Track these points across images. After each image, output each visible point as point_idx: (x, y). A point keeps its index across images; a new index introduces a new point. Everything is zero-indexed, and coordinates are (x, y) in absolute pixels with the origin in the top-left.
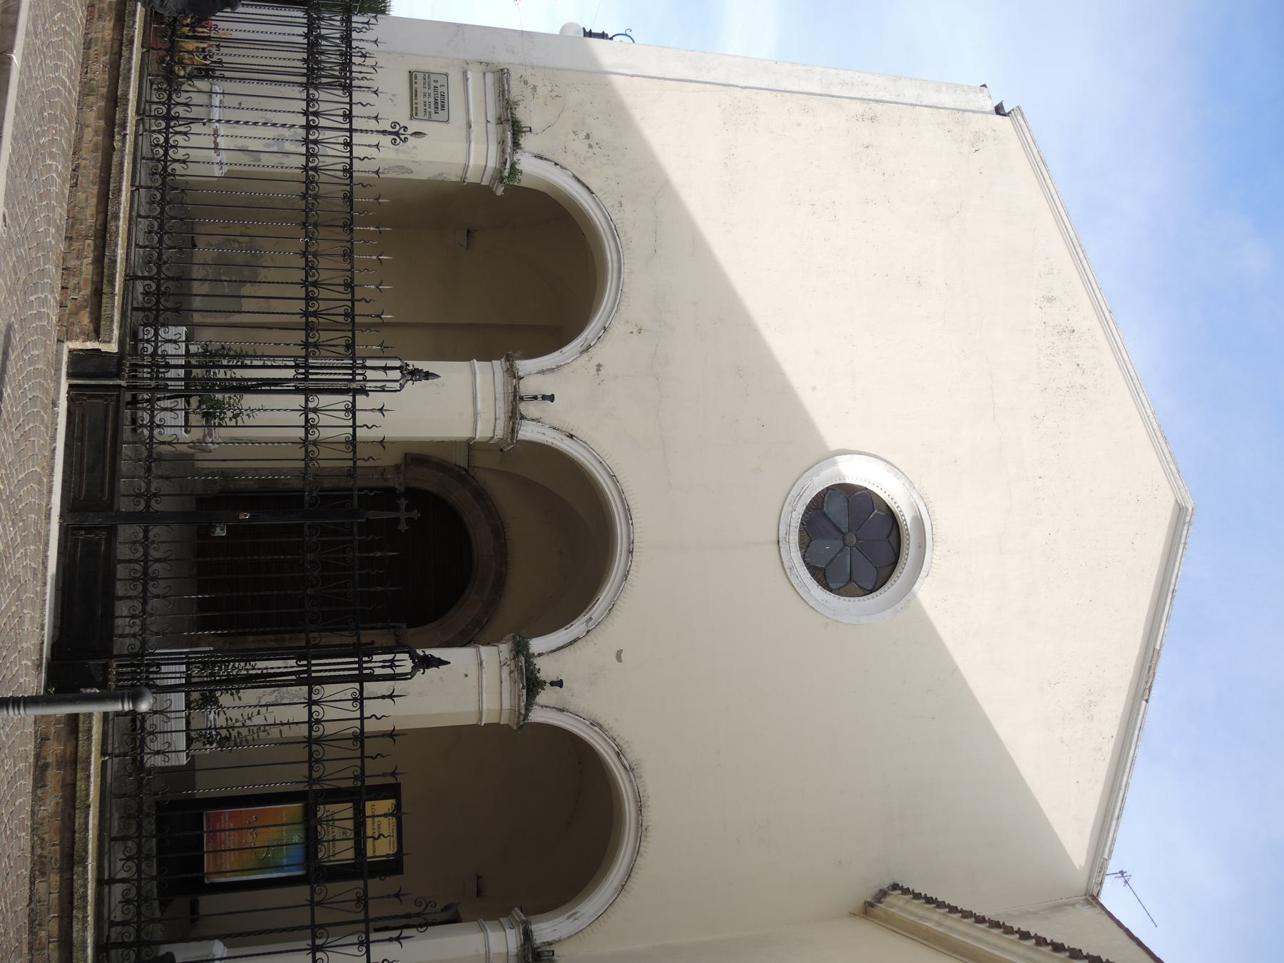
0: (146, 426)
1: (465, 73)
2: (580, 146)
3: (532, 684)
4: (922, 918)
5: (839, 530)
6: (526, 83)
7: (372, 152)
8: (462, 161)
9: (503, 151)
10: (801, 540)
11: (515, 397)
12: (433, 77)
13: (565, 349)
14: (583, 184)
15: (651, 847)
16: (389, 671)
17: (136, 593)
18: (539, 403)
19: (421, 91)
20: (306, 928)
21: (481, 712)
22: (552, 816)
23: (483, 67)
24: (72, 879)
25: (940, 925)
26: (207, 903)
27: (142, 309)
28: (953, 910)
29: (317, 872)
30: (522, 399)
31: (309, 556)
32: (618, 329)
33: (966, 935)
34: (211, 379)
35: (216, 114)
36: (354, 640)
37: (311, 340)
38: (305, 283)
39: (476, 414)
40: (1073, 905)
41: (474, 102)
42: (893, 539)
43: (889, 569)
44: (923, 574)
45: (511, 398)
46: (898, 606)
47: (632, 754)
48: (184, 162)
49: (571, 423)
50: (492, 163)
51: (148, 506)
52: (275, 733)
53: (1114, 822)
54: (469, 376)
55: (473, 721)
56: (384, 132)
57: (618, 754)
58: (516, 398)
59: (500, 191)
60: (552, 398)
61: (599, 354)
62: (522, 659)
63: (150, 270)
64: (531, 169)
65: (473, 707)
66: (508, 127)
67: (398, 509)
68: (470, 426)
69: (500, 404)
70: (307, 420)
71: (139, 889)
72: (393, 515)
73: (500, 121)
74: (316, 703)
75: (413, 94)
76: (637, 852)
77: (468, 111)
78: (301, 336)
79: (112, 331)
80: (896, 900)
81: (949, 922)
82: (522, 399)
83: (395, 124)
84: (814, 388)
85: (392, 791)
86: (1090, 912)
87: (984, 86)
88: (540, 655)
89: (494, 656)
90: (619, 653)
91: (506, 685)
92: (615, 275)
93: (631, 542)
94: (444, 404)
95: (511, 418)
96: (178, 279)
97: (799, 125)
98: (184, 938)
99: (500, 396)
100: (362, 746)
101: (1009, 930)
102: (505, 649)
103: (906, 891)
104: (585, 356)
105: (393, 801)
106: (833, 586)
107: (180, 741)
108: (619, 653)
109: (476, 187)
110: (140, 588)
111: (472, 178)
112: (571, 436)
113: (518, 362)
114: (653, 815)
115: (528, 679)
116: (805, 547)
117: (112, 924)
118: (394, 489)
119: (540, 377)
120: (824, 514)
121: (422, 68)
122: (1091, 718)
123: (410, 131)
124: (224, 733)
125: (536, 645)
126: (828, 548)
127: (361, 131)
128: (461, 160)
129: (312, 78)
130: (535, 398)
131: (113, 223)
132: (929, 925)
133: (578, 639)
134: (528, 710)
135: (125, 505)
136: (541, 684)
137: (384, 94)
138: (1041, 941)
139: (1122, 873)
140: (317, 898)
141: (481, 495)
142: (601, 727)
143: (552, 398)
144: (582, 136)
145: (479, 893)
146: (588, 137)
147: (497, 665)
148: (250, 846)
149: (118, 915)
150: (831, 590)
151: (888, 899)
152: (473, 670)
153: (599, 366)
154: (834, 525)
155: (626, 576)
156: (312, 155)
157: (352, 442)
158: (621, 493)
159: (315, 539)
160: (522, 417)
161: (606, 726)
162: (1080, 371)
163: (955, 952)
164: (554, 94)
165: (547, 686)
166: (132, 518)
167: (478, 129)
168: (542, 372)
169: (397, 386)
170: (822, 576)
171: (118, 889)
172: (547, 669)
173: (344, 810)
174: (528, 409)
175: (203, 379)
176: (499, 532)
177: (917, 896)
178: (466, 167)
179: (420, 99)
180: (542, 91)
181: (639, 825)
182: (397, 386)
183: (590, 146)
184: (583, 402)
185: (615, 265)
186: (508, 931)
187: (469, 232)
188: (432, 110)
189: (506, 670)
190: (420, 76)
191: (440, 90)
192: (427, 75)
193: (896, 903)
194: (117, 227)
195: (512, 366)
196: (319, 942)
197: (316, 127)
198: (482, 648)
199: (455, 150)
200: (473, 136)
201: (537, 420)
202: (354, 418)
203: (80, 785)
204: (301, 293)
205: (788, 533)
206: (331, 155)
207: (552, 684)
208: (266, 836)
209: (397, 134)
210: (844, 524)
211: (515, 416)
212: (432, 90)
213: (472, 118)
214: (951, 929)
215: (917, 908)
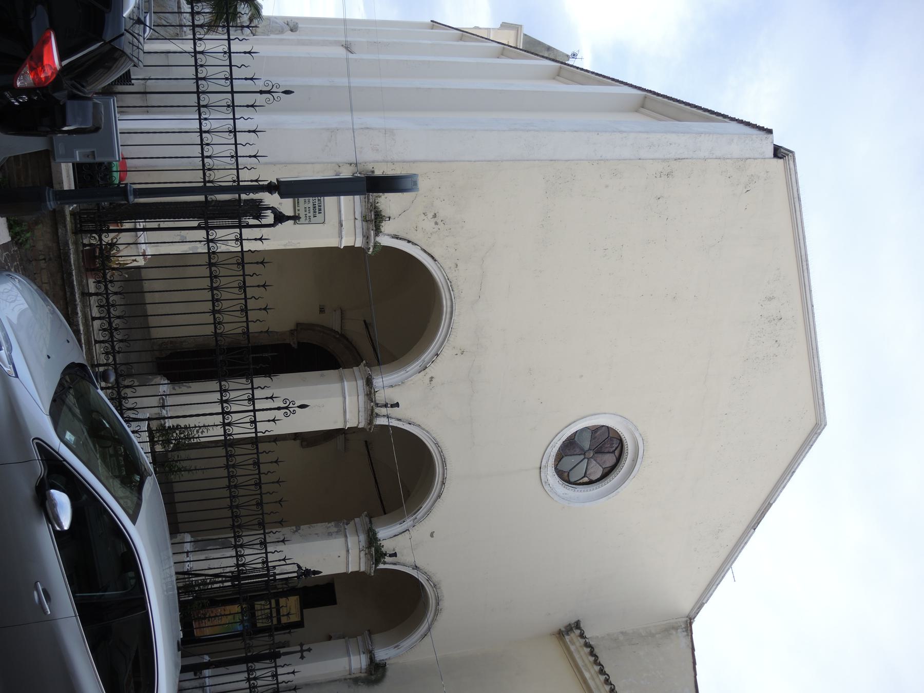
2: (428, 225)
7: (291, 677)
14: (429, 254)
31: (221, 358)
32: (447, 353)
37: (212, 261)
38: (227, 467)
45: (369, 412)
56: (279, 408)
60: (397, 405)
61: (432, 370)
68: (341, 419)
69: (362, 414)
70: (211, 273)
74: (217, 288)
78: (246, 675)
92: (448, 316)
93: (444, 478)
99: (362, 409)
114: (445, 604)
119: (391, 389)
143: (397, 405)
144: (430, 215)
146: (435, 216)
152: (343, 553)
156: (236, 517)
157: (247, 333)
162: (777, 345)
172: (388, 546)
183: (436, 223)
185: (449, 310)
188: (312, 214)
189: (363, 553)
198: (337, 327)
200: (343, 233)
202: (247, 316)
204: (210, 319)
206: (221, 147)
209: (287, 408)
211: (372, 415)
213: (343, 218)
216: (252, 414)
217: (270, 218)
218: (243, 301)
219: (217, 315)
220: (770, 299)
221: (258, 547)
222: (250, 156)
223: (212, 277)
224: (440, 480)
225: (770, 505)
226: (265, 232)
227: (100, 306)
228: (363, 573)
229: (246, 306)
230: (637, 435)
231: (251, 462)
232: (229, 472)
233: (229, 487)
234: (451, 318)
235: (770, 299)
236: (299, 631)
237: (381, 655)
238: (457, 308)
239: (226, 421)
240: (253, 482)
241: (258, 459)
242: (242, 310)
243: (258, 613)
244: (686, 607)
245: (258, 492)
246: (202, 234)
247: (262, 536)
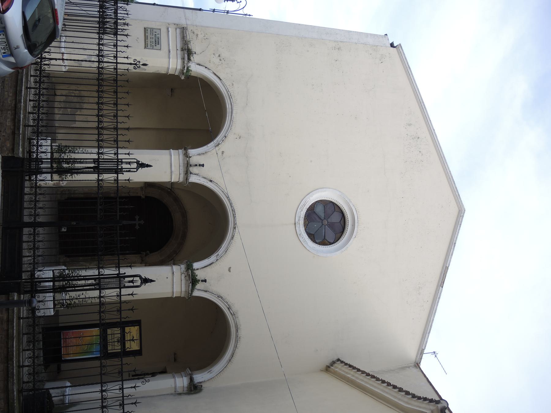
0: (35, 145)
1: (168, 29)
2: (216, 60)
3: (194, 281)
4: (347, 373)
5: (320, 219)
6: (193, 33)
8: (166, 66)
9: (184, 62)
10: (304, 223)
11: (188, 165)
12: (154, 30)
13: (209, 145)
14: (217, 76)
15: (242, 345)
16: (131, 284)
17: (30, 254)
18: (198, 167)
19: (149, 36)
20: (101, 377)
21: (173, 293)
22: (200, 336)
23: (175, 26)
24: (8, 367)
25: (353, 376)
26: (64, 366)
27: (33, 101)
28: (359, 370)
29: (106, 355)
30: (191, 165)
31: (100, 239)
32: (231, 137)
33: (362, 380)
34: (61, 159)
35: (63, 45)
36: (117, 272)
39: (171, 172)
40: (409, 367)
41: (171, 41)
42: (342, 222)
43: (340, 234)
44: (353, 236)
46: (343, 249)
47: (234, 309)
48: (48, 77)
49: (211, 176)
50: (179, 67)
51: (35, 219)
52: (89, 301)
53: (427, 335)
54: (168, 157)
55: (170, 296)
56: (131, 64)
57: (229, 309)
58: (188, 165)
59: (183, 78)
60: (203, 165)
61: (223, 147)
62: (190, 271)
63: (31, 190)
64: (195, 69)
65: (170, 290)
66: (186, 52)
67: (135, 220)
68: (169, 177)
69: (182, 168)
71: (34, 369)
72: (133, 222)
73: (182, 50)
74: (103, 312)
75: (146, 38)
76: (236, 347)
77: (169, 45)
79: (19, 149)
80: (338, 365)
81: (357, 375)
82: (191, 165)
83: (135, 60)
84: (311, 161)
85: (137, 323)
86: (415, 370)
87: (386, 35)
88: (197, 269)
89: (178, 270)
90: (230, 268)
91: (183, 282)
93: (235, 224)
94: (161, 166)
95: (186, 174)
96: (46, 126)
97: (308, 51)
98: (55, 379)
99: (182, 165)
100: (121, 314)
101: (378, 379)
102: (183, 267)
103: (342, 362)
104: (217, 148)
105: (138, 327)
106: (317, 241)
107: (51, 304)
108: (230, 268)
109: (173, 75)
110: (32, 252)
111: (171, 72)
112: (211, 181)
113: (189, 150)
115: (192, 279)
116: (306, 226)
117: (24, 382)
118: (140, 197)
119: (198, 157)
120: (315, 212)
121: (150, 26)
122: (419, 294)
123: (141, 63)
124: (68, 302)
125: (196, 265)
126: (316, 226)
127: (121, 63)
128: (166, 66)
129: (102, 30)
130: (196, 165)
131: (19, 105)
132: (349, 376)
133: (213, 263)
134: (192, 291)
135: (26, 219)
136: (198, 281)
137: (134, 33)
138: (389, 384)
139: (434, 352)
140: (103, 372)
141: (177, 199)
142: (222, 298)
143: (203, 165)
144: (217, 55)
145: (175, 360)
146: (219, 56)
147: (180, 274)
148: (81, 344)
149: (26, 379)
150: (316, 243)
151: (335, 365)
152: (170, 275)
153: (223, 152)
154: (319, 217)
155: (232, 238)
158: (231, 204)
159: (102, 232)
160: (191, 173)
161: (224, 297)
162: (421, 154)
163: (358, 387)
164: (205, 38)
165: (200, 282)
166: (29, 225)
167: (173, 53)
168: (199, 154)
169: (135, 170)
170: (312, 237)
171: (26, 369)
172: (200, 275)
173: (117, 331)
174: (193, 170)
175: (58, 159)
176: (184, 214)
177: (346, 364)
178: (168, 68)
179: (149, 40)
180: (200, 36)
181: (237, 336)
182: (135, 170)
183: (220, 60)
184: (215, 167)
185: (230, 110)
186: (184, 378)
187: (172, 90)
188: (154, 44)
189: (183, 276)
190: (149, 30)
191: (157, 36)
192: (152, 29)
193: (338, 367)
194: (21, 106)
195: (186, 152)
196: (104, 389)
197: (103, 62)
199: (163, 61)
200: (171, 56)
201: (197, 174)
203: (10, 331)
204: (96, 119)
205: (299, 220)
207: (202, 281)
208: (87, 340)
209: (136, 64)
210: (322, 215)
211: (187, 173)
212: (154, 36)
213: (171, 48)
214: (357, 378)
215: (346, 369)
217: (138, 282)
218: (120, 366)
219: (100, 143)
220: (410, 125)
221: (112, 106)
222: (129, 295)
223: (99, 109)
224: (232, 226)
225: (447, 268)
226: (135, 290)
227: (34, 120)
228: (184, 297)
229: (120, 308)
230: (352, 206)
231: (112, 114)
232: (99, 95)
233: (98, 128)
234: (232, 115)
235: (410, 125)
236: (138, 357)
237: (199, 377)
238: (235, 108)
239: (100, 66)
240: (112, 139)
241: (117, 89)
242: (118, 311)
243: (109, 337)
244: (412, 354)
245: (115, 109)
246: (96, 150)
247: (115, 111)
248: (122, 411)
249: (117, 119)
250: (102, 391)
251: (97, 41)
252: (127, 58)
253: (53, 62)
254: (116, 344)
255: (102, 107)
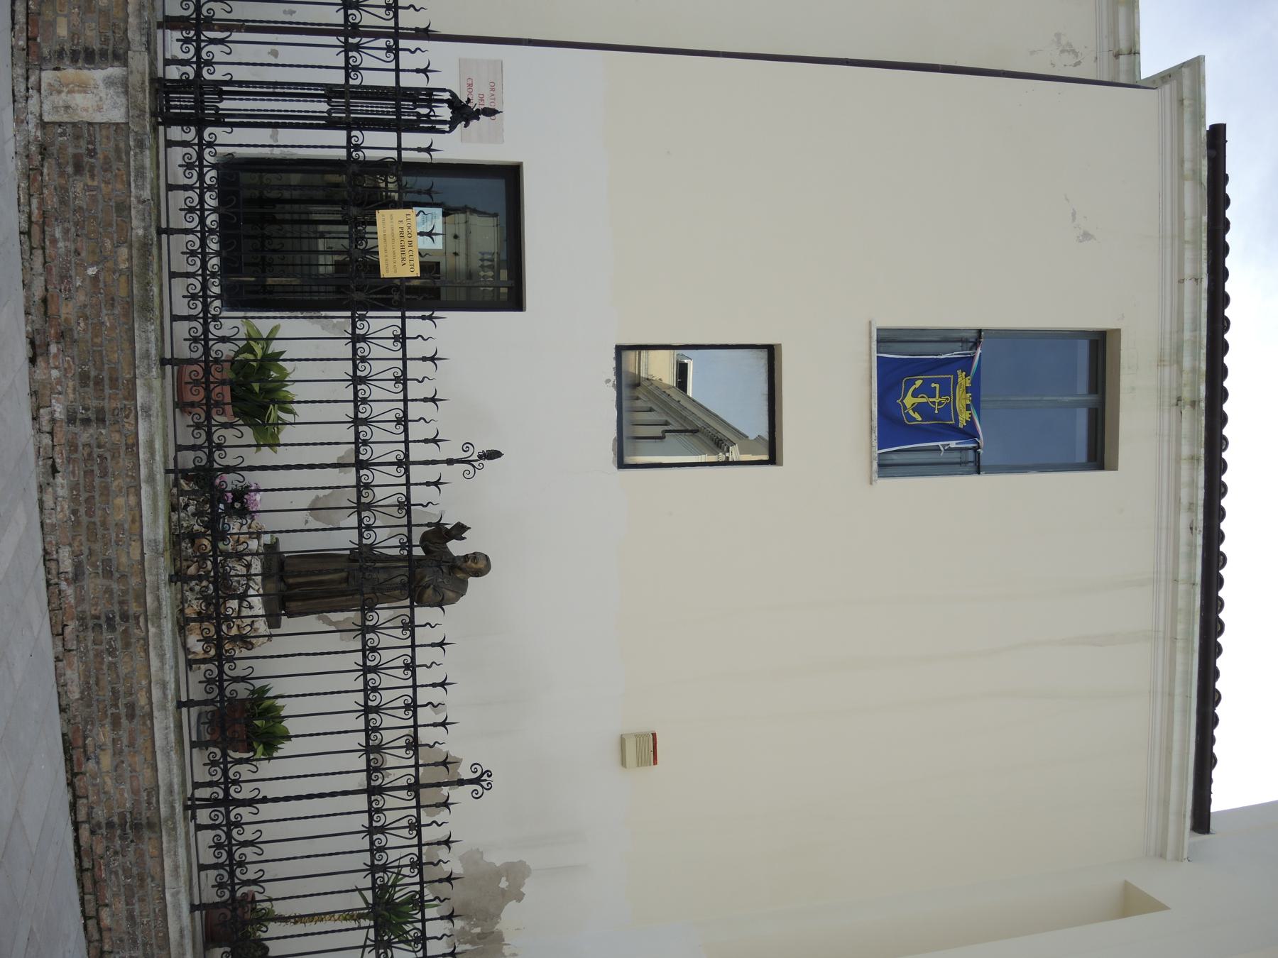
74: (366, 422)
182: (446, 127)
216: (412, 771)
248: (420, 954)
249: (397, 58)
250: (364, 630)
251: (366, 857)
252: (435, 441)
253: (267, 811)
254: (406, 871)
255: (380, 801)
